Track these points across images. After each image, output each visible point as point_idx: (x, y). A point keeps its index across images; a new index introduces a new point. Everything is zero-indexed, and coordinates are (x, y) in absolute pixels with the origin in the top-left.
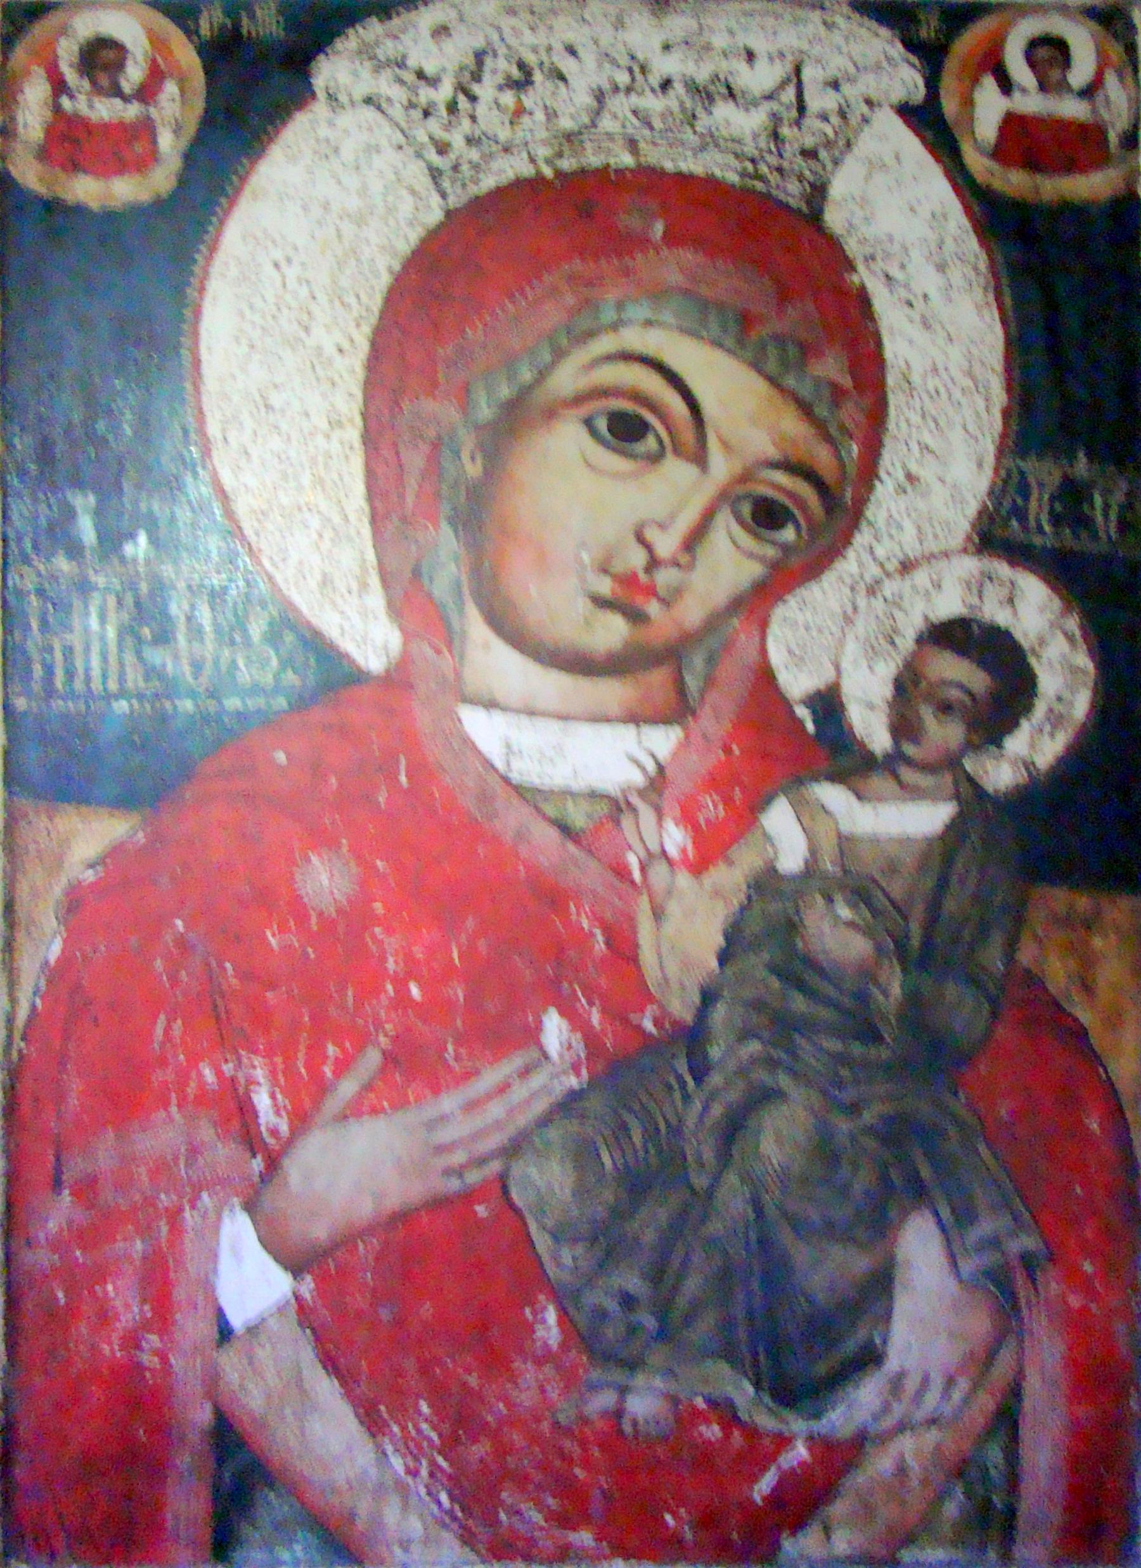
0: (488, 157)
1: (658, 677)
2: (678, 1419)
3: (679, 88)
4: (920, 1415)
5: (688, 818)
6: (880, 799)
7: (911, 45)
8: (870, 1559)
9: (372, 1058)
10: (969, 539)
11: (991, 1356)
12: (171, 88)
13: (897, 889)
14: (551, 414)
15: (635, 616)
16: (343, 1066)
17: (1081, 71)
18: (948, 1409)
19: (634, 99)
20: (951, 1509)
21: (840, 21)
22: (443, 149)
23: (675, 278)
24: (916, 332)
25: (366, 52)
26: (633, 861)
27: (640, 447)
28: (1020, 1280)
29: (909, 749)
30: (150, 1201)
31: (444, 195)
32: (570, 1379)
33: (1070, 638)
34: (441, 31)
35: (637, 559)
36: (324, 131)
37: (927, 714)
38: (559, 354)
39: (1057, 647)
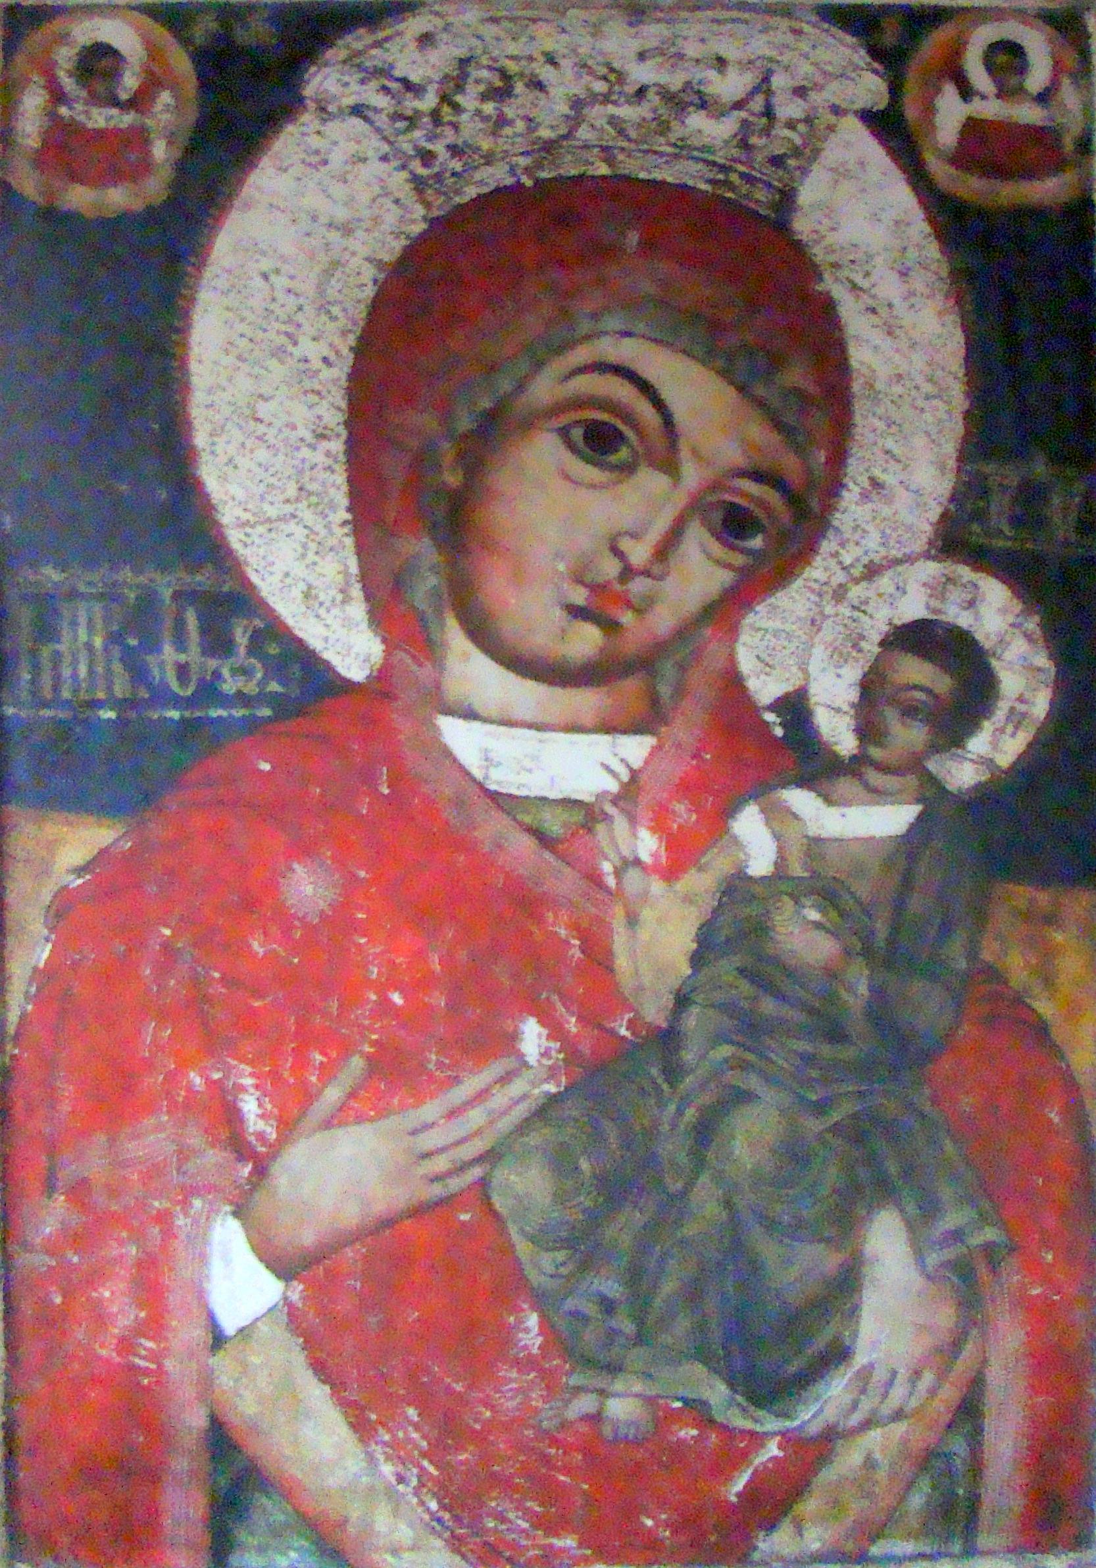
0: (469, 169)
1: (631, 685)
2: (657, 1422)
3: (652, 95)
4: (886, 1410)
5: (659, 825)
6: (847, 803)
7: (875, 52)
8: (839, 1555)
9: (357, 1063)
10: (930, 543)
11: (955, 1346)
12: (165, 97)
13: (863, 889)
14: (529, 423)
15: (610, 626)
16: (327, 1073)
17: (1038, 76)
18: (914, 1403)
19: (611, 109)
20: (917, 1501)
21: (807, 28)
22: (427, 157)
23: (647, 287)
24: (877, 338)
25: (353, 61)
26: (607, 867)
27: (614, 458)
28: (982, 1270)
29: (875, 753)
30: (142, 1205)
31: (428, 206)
32: (551, 1383)
33: (1028, 637)
34: (426, 40)
35: (610, 568)
36: (315, 142)
37: (891, 715)
38: (538, 365)
39: (1018, 647)
